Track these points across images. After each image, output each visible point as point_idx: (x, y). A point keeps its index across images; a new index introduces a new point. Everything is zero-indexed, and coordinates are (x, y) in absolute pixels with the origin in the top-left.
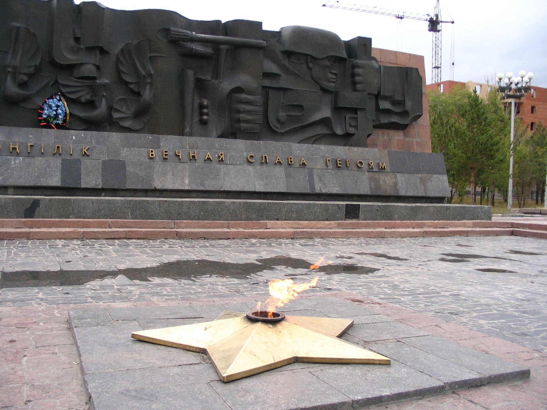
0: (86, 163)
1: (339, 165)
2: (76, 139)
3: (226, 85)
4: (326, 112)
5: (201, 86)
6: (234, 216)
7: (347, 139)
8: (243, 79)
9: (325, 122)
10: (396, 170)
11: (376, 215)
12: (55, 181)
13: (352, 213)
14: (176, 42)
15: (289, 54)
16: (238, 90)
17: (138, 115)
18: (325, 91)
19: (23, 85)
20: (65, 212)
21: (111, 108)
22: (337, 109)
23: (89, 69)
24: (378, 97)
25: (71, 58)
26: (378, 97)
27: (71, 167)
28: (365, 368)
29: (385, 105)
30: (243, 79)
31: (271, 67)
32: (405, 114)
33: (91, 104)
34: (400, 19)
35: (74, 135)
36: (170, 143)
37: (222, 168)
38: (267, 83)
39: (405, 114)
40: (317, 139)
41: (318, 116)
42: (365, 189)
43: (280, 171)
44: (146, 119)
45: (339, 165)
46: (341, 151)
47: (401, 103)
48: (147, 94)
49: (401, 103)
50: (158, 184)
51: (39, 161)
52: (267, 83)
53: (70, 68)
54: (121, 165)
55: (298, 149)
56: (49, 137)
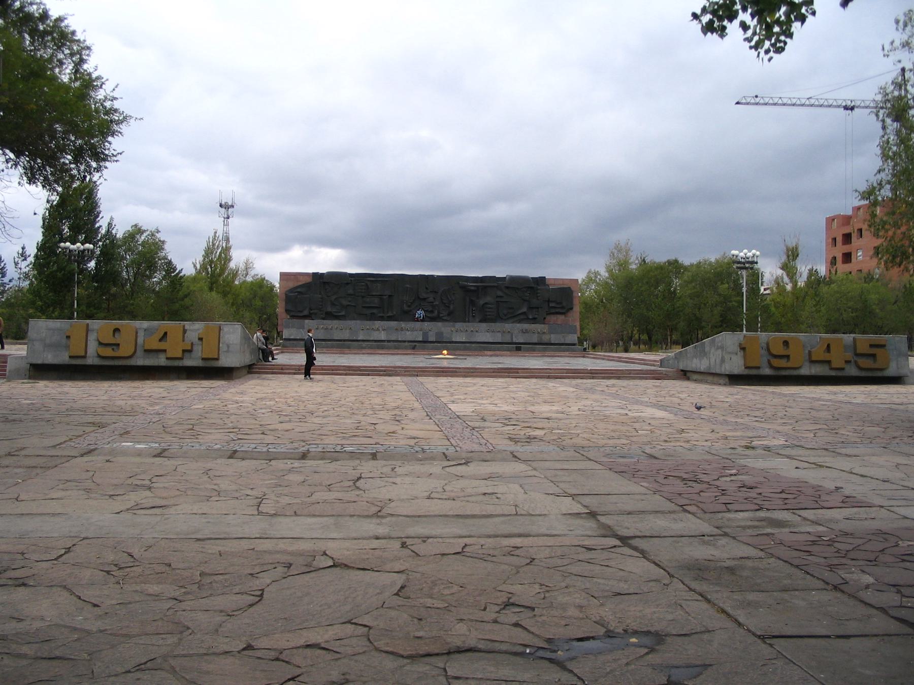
0: (430, 333)
1: (525, 332)
2: (426, 325)
3: (482, 302)
4: (524, 310)
5: (472, 303)
6: (476, 350)
7: (534, 321)
8: (489, 299)
9: (524, 313)
10: (550, 333)
11: (528, 350)
12: (421, 339)
13: (518, 349)
14: (463, 288)
15: (507, 288)
16: (486, 303)
17: (449, 315)
18: (525, 300)
19: (409, 306)
20: (424, 349)
21: (439, 313)
22: (531, 308)
23: (431, 299)
24: (549, 301)
25: (425, 296)
26: (549, 301)
27: (425, 334)
28: (861, 638)
29: (552, 305)
30: (489, 299)
31: (499, 293)
32: (563, 308)
33: (432, 312)
34: (850, 112)
35: (426, 324)
36: (459, 325)
37: (477, 334)
38: (499, 299)
39: (563, 308)
40: (520, 321)
41: (520, 312)
42: (535, 341)
43: (499, 335)
44: (452, 317)
45: (525, 332)
46: (526, 326)
47: (560, 303)
48: (452, 307)
49: (560, 303)
50: (454, 340)
51: (415, 333)
52: (499, 299)
53: (425, 299)
54: (442, 333)
55: (508, 326)
56: (418, 324)
